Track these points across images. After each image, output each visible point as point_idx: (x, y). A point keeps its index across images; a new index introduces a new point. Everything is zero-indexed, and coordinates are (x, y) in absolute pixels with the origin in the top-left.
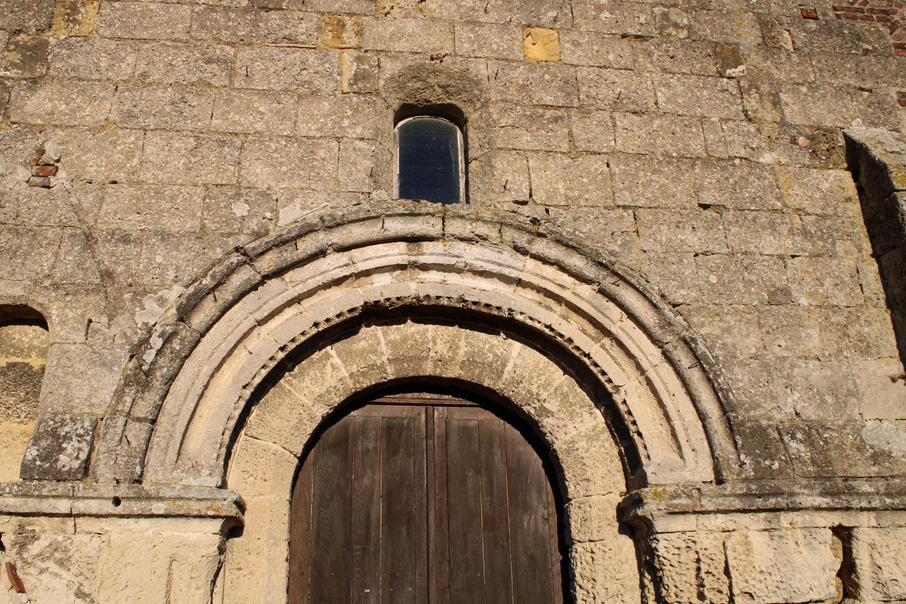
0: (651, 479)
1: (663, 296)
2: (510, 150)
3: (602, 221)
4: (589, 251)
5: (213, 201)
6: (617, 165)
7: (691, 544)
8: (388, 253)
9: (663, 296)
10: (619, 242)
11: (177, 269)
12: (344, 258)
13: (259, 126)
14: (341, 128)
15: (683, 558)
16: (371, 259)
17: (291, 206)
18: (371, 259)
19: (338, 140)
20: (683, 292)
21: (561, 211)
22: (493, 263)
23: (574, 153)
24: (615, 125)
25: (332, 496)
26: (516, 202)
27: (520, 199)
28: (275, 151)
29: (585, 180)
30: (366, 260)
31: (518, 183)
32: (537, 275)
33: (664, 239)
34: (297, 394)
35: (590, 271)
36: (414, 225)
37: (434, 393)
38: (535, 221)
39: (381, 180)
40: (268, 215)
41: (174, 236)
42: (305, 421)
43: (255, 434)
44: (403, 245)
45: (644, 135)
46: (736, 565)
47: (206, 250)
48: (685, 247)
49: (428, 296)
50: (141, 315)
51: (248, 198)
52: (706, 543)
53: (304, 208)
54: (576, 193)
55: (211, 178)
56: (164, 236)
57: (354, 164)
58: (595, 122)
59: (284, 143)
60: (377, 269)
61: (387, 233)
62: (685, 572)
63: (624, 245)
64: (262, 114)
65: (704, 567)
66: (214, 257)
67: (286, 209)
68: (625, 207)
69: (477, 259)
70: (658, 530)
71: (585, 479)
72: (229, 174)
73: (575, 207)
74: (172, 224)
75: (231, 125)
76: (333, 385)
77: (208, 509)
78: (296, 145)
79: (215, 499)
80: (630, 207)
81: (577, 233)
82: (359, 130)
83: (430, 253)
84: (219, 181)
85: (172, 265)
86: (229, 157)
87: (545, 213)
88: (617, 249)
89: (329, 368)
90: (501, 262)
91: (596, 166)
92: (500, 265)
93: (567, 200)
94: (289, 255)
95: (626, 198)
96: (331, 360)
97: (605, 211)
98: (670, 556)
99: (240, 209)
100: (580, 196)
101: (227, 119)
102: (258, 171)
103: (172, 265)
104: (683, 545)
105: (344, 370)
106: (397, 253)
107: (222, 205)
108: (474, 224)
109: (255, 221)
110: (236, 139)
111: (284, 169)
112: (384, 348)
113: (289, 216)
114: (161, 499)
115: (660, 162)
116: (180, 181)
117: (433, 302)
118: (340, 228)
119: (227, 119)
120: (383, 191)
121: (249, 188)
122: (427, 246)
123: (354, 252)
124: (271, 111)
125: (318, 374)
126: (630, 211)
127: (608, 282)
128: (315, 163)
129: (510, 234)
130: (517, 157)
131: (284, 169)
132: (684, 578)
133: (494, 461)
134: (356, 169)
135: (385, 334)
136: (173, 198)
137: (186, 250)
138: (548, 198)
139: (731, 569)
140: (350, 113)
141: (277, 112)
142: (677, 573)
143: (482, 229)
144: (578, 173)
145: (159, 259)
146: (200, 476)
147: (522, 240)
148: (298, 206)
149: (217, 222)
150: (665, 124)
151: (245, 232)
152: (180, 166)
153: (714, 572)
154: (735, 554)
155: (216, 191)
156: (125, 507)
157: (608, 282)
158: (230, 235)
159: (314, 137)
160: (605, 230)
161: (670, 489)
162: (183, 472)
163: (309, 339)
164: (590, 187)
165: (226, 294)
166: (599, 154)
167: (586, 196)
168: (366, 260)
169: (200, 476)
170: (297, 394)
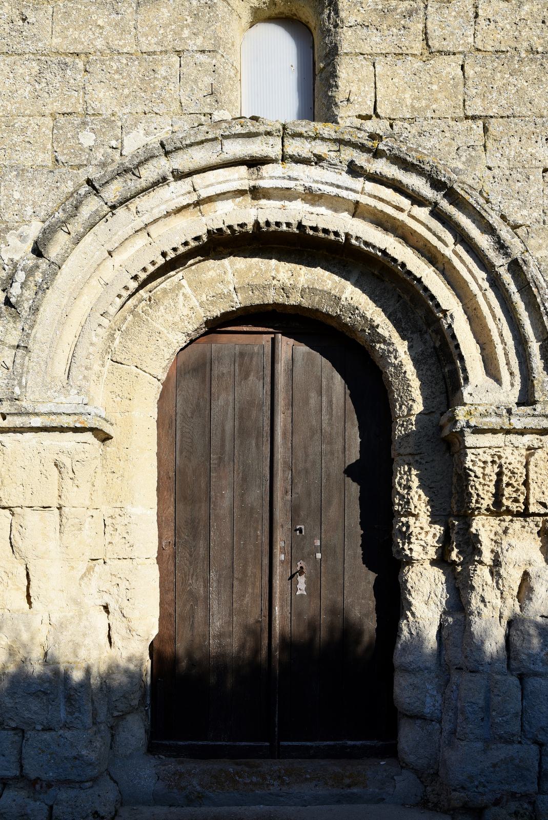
0: (467, 398)
1: (503, 217)
2: (357, 54)
3: (447, 134)
4: (428, 168)
5: (61, 132)
6: (473, 67)
7: (496, 459)
8: (228, 178)
9: (503, 217)
10: (464, 159)
11: (34, 204)
12: (185, 185)
13: (100, 44)
14: (181, 39)
15: (488, 471)
16: (212, 185)
17: (134, 132)
18: (212, 185)
19: (178, 53)
20: (525, 212)
21: (406, 125)
22: (332, 185)
23: (431, 52)
24: (477, 16)
25: (193, 414)
26: (360, 117)
27: (364, 113)
28: (117, 72)
29: (435, 87)
30: (208, 186)
31: (363, 94)
32: (375, 197)
33: (513, 153)
34: (154, 323)
35: (426, 191)
36: (253, 147)
37: (269, 328)
38: (373, 137)
39: (223, 98)
40: (114, 143)
41: (28, 171)
42: (162, 348)
43: (119, 360)
44: (243, 169)
45: (508, 27)
46: (535, 478)
47: (58, 184)
48: (534, 162)
49: (268, 223)
50: (6, 251)
51: (94, 126)
52: (511, 459)
53: (147, 134)
54: (424, 103)
55: (57, 107)
56: (21, 171)
57: (195, 81)
58: (454, 14)
59: (125, 61)
60: (218, 195)
61: (227, 156)
62: (488, 483)
63: (469, 161)
64: (101, 27)
65: (505, 479)
66: (66, 190)
67: (131, 135)
68: (474, 118)
69: (317, 182)
70: (467, 444)
71: (411, 399)
72: (74, 102)
73: (421, 120)
74: (25, 158)
75: (71, 44)
76: (185, 314)
77: (75, 421)
78: (136, 63)
79: (82, 414)
80: (480, 117)
81: (420, 149)
82: (199, 41)
83: (271, 176)
84: (65, 110)
85: (28, 200)
86: (72, 81)
87: (389, 128)
88: (461, 166)
89: (181, 297)
90: (340, 184)
91: (448, 69)
92: (338, 187)
93: (412, 112)
94: (134, 184)
95: (476, 108)
96: (183, 290)
97: (452, 123)
98: (475, 468)
99: (87, 139)
100: (428, 107)
101: (67, 37)
102: (101, 95)
103: (28, 200)
104: (489, 459)
105: (194, 299)
106: (239, 177)
107: (69, 135)
108: (313, 143)
109: (102, 151)
110: (77, 60)
111: (126, 91)
112: (229, 277)
113: (134, 142)
114: (37, 414)
115: (521, 61)
116: (28, 112)
117: (273, 228)
118: (180, 152)
119: (67, 37)
120: (226, 112)
121: (94, 115)
122: (267, 170)
123: (196, 178)
124: (110, 24)
125: (172, 304)
126: (480, 123)
127: (445, 205)
128: (156, 83)
129: (349, 154)
130: (364, 62)
131: (126, 91)
132: (486, 488)
133: (334, 384)
134: (198, 87)
135: (232, 264)
136: (23, 130)
137: (40, 185)
138: (393, 110)
139: (530, 481)
140: (190, 20)
141: (116, 24)
142: (480, 483)
143: (321, 148)
144: (428, 79)
145: (17, 195)
146: (69, 395)
147: (362, 159)
148: (142, 132)
149: (66, 154)
150: (535, 10)
151: (93, 163)
152: (26, 94)
153: (515, 484)
154: (536, 469)
155: (62, 120)
156: (9, 422)
157: (445, 205)
158: (79, 166)
159: (154, 53)
160: (449, 145)
161: (481, 409)
162: (55, 392)
163: (158, 268)
164: (439, 96)
165: (76, 226)
166: (454, 54)
167: (434, 106)
168: (208, 186)
169: (69, 395)
170: (154, 323)
